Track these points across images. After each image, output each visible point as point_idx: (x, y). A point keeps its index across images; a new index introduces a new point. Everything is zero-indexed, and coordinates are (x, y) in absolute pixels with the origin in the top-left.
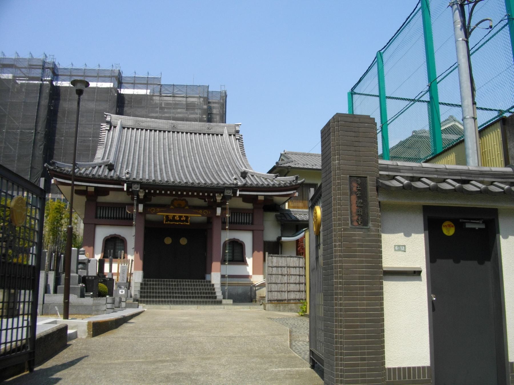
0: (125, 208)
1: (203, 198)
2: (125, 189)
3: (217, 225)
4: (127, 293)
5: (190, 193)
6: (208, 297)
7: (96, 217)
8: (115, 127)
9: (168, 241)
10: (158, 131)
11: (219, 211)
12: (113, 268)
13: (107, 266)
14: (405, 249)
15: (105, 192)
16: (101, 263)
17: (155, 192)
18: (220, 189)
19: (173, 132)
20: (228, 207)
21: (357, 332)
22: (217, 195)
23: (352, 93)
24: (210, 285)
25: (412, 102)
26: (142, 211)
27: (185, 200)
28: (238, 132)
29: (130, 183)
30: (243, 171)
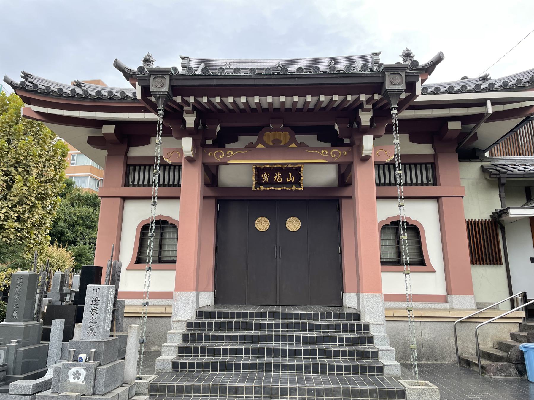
3: (365, 179)
7: (126, 185)
9: (262, 224)
26: (190, 154)
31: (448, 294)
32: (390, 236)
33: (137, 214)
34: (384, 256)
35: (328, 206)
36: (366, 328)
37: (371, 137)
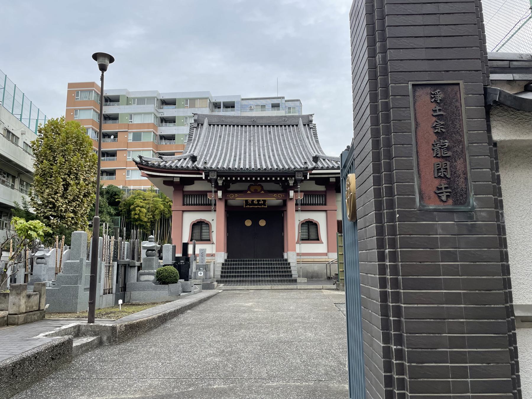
0: (207, 195)
1: (276, 182)
2: (204, 178)
3: (291, 206)
4: (205, 274)
5: (244, 179)
6: (283, 275)
7: (184, 205)
8: (202, 125)
9: (248, 223)
10: (244, 126)
11: (292, 193)
17: (261, 179)
18: (291, 173)
19: (254, 126)
20: (299, 190)
22: (288, 179)
26: (221, 197)
28: (311, 121)
29: (208, 172)
30: (315, 155)
31: (328, 251)
32: (306, 228)
33: (189, 218)
34: (303, 236)
35: (277, 216)
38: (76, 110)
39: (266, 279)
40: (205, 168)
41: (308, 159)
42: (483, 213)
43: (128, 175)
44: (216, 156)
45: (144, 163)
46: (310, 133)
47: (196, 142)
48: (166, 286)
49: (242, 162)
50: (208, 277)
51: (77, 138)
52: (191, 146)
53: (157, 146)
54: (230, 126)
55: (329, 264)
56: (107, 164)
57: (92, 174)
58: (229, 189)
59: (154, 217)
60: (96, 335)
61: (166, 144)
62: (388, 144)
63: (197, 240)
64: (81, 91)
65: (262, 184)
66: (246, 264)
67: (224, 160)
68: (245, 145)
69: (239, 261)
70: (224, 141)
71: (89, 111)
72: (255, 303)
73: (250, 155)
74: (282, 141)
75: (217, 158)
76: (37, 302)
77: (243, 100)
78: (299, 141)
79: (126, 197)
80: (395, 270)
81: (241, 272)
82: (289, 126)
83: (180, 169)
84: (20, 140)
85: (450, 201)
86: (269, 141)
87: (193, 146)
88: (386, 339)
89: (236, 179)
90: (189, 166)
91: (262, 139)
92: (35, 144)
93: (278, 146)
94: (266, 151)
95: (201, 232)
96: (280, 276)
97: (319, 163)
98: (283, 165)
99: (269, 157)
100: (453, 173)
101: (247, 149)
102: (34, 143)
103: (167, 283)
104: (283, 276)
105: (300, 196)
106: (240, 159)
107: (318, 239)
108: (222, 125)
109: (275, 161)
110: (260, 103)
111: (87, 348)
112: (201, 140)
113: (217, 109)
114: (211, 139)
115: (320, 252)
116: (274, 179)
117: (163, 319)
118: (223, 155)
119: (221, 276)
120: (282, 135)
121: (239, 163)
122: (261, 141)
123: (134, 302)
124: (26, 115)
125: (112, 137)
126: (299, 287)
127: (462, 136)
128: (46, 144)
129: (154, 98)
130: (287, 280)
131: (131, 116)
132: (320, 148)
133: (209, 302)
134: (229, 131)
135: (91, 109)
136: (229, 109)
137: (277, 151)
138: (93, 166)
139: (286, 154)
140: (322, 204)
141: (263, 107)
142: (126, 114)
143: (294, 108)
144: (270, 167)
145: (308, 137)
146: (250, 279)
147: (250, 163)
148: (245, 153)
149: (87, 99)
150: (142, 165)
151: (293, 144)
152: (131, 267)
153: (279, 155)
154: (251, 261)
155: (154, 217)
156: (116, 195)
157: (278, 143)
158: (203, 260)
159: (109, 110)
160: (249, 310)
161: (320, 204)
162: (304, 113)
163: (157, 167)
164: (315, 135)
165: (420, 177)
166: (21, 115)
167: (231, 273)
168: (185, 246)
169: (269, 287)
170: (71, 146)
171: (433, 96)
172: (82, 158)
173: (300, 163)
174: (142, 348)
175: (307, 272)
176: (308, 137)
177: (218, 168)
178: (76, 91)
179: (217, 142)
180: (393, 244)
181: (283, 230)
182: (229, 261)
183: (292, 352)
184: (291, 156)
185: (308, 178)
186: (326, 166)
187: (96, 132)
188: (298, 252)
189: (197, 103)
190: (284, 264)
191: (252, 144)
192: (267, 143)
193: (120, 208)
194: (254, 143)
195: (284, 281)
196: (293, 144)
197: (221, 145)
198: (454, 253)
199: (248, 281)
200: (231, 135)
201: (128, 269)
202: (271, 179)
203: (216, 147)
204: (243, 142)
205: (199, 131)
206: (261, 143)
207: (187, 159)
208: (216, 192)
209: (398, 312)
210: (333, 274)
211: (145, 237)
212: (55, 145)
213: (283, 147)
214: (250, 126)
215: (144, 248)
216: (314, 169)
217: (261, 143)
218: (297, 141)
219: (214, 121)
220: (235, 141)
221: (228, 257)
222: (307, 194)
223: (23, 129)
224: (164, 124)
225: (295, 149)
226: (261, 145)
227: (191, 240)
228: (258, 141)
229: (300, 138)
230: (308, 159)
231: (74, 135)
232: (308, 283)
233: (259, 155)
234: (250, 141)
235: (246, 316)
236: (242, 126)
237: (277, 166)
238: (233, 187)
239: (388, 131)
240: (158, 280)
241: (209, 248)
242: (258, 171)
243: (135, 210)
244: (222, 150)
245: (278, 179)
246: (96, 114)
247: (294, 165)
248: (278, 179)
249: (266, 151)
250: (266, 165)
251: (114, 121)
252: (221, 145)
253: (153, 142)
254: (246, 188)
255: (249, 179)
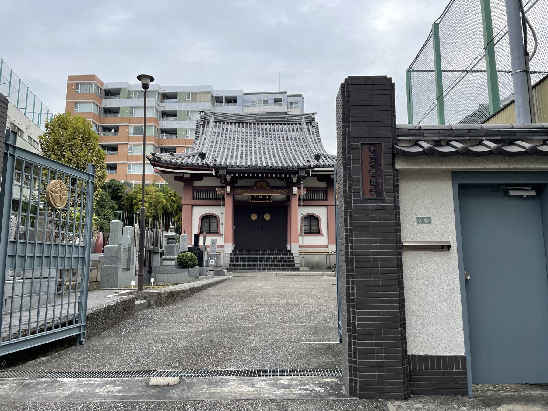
1: (281, 178)
2: (214, 174)
3: (294, 202)
4: (217, 262)
6: (287, 264)
7: (193, 199)
8: (208, 122)
9: (254, 217)
11: (295, 189)
12: (207, 241)
13: (201, 239)
14: (417, 220)
15: (200, 177)
16: (197, 237)
19: (258, 124)
20: (302, 186)
21: (372, 314)
22: (292, 176)
23: (409, 72)
24: (290, 254)
25: (464, 73)
27: (266, 181)
28: (314, 120)
29: (218, 169)
31: (328, 244)
32: (308, 221)
33: (199, 212)
35: (281, 211)
36: (292, 254)
37: (296, 187)
38: (77, 103)
39: (271, 267)
40: (215, 165)
41: (311, 156)
42: (389, 201)
43: (129, 169)
44: (223, 153)
45: (157, 160)
46: (313, 131)
47: (203, 139)
48: (187, 269)
49: (249, 159)
50: (219, 265)
51: (84, 132)
52: (198, 143)
53: (158, 140)
54: (235, 123)
55: (329, 255)
56: (110, 159)
57: (98, 169)
58: (236, 185)
59: (156, 212)
60: (145, 299)
61: (167, 138)
62: (350, 170)
63: (207, 233)
64: (82, 84)
65: (267, 180)
66: (253, 254)
67: (232, 158)
68: (251, 143)
69: (246, 251)
70: (230, 139)
71: (90, 104)
72: (263, 287)
73: (255, 153)
74: (285, 139)
75: (225, 155)
76: (95, 275)
77: (245, 94)
78: (301, 139)
79: (129, 191)
80: (351, 225)
81: (248, 261)
82: (292, 124)
83: (190, 166)
84: (25, 133)
85: (375, 195)
86: (273, 139)
87: (200, 143)
88: (347, 254)
89: (244, 175)
90: (199, 162)
91: (267, 136)
92: (42, 139)
93: (282, 144)
94: (270, 148)
95: (210, 225)
96: (284, 265)
97: (320, 161)
98: (287, 163)
99: (274, 155)
100: (377, 183)
101: (253, 147)
102: (41, 138)
103: (188, 267)
104: (287, 265)
105: (303, 192)
106: (246, 156)
107: (319, 232)
108: (228, 123)
109: (280, 159)
110: (263, 98)
111: (142, 307)
112: (208, 138)
113: (219, 104)
114: (218, 136)
115: (322, 244)
116: (278, 176)
117: (193, 291)
118: (230, 152)
119: (230, 265)
120: (286, 133)
121: (246, 160)
122: (265, 139)
123: (159, 283)
124: (30, 109)
125: (113, 131)
126: (301, 274)
127: (381, 167)
128: (53, 139)
129: (155, 91)
130: (290, 269)
131: (132, 109)
132: (321, 146)
133: (224, 284)
134: (235, 129)
135: (91, 102)
136: (231, 104)
137: (281, 148)
138: (99, 161)
139: (289, 152)
140: (323, 200)
141: (265, 101)
142: (127, 108)
143: (296, 103)
144: (275, 165)
145: (310, 136)
146: (256, 267)
147: (256, 160)
148: (251, 151)
149: (87, 92)
150: (155, 161)
151: (296, 142)
152: (155, 253)
153: (283, 153)
154: (257, 251)
155: (156, 212)
156: (118, 189)
157: (282, 141)
158: (214, 250)
159: (111, 103)
160: (261, 287)
161: (321, 200)
162: (307, 111)
163: (169, 164)
164: (317, 133)
165: (363, 184)
166: (25, 109)
167: (238, 263)
168: (197, 237)
169: (274, 273)
170: (78, 141)
171: (370, 149)
172: (88, 153)
173: (303, 161)
174: (182, 309)
175: (309, 262)
176: (310, 136)
177: (227, 165)
178: (76, 83)
179: (223, 140)
180: (350, 214)
181: (286, 224)
182: (236, 251)
183: (299, 310)
184: (294, 154)
185: (311, 175)
186: (327, 164)
187: (96, 126)
188: (300, 244)
189: (199, 97)
190: (287, 254)
191: (257, 141)
192: (271, 140)
193: (122, 203)
194: (259, 141)
195: (288, 269)
196: (296, 142)
197: (227, 142)
198: (376, 217)
199: (255, 269)
200: (236, 132)
201: (153, 255)
202: (276, 176)
203: (223, 145)
204: (248, 140)
205: (205, 128)
206: (265, 141)
207: (197, 156)
208: (225, 187)
209: (352, 242)
210: (332, 264)
211: (166, 229)
212: (62, 140)
213: (287, 144)
214: (254, 124)
215: (166, 237)
216: (316, 166)
217: (265, 141)
218: (300, 139)
219: (220, 118)
220: (240, 139)
221: (235, 248)
222: (310, 190)
223: (27, 123)
224: (165, 118)
225: (298, 147)
226: (266, 143)
227: (201, 232)
228: (263, 139)
229: (302, 136)
230: (311, 156)
231: (81, 130)
232: (309, 271)
233: (265, 153)
234: (255, 139)
235: (259, 291)
236: (247, 124)
237: (282, 163)
238: (240, 183)
239: (350, 165)
240: (179, 264)
241: (220, 241)
242: (265, 168)
243: (137, 204)
244: (229, 147)
245: (283, 176)
246: (96, 107)
247: (297, 162)
248: (283, 176)
249: (270, 148)
250: (272, 163)
251: (115, 115)
252: (227, 142)
253: (155, 136)
254: (253, 185)
255: (255, 175)
